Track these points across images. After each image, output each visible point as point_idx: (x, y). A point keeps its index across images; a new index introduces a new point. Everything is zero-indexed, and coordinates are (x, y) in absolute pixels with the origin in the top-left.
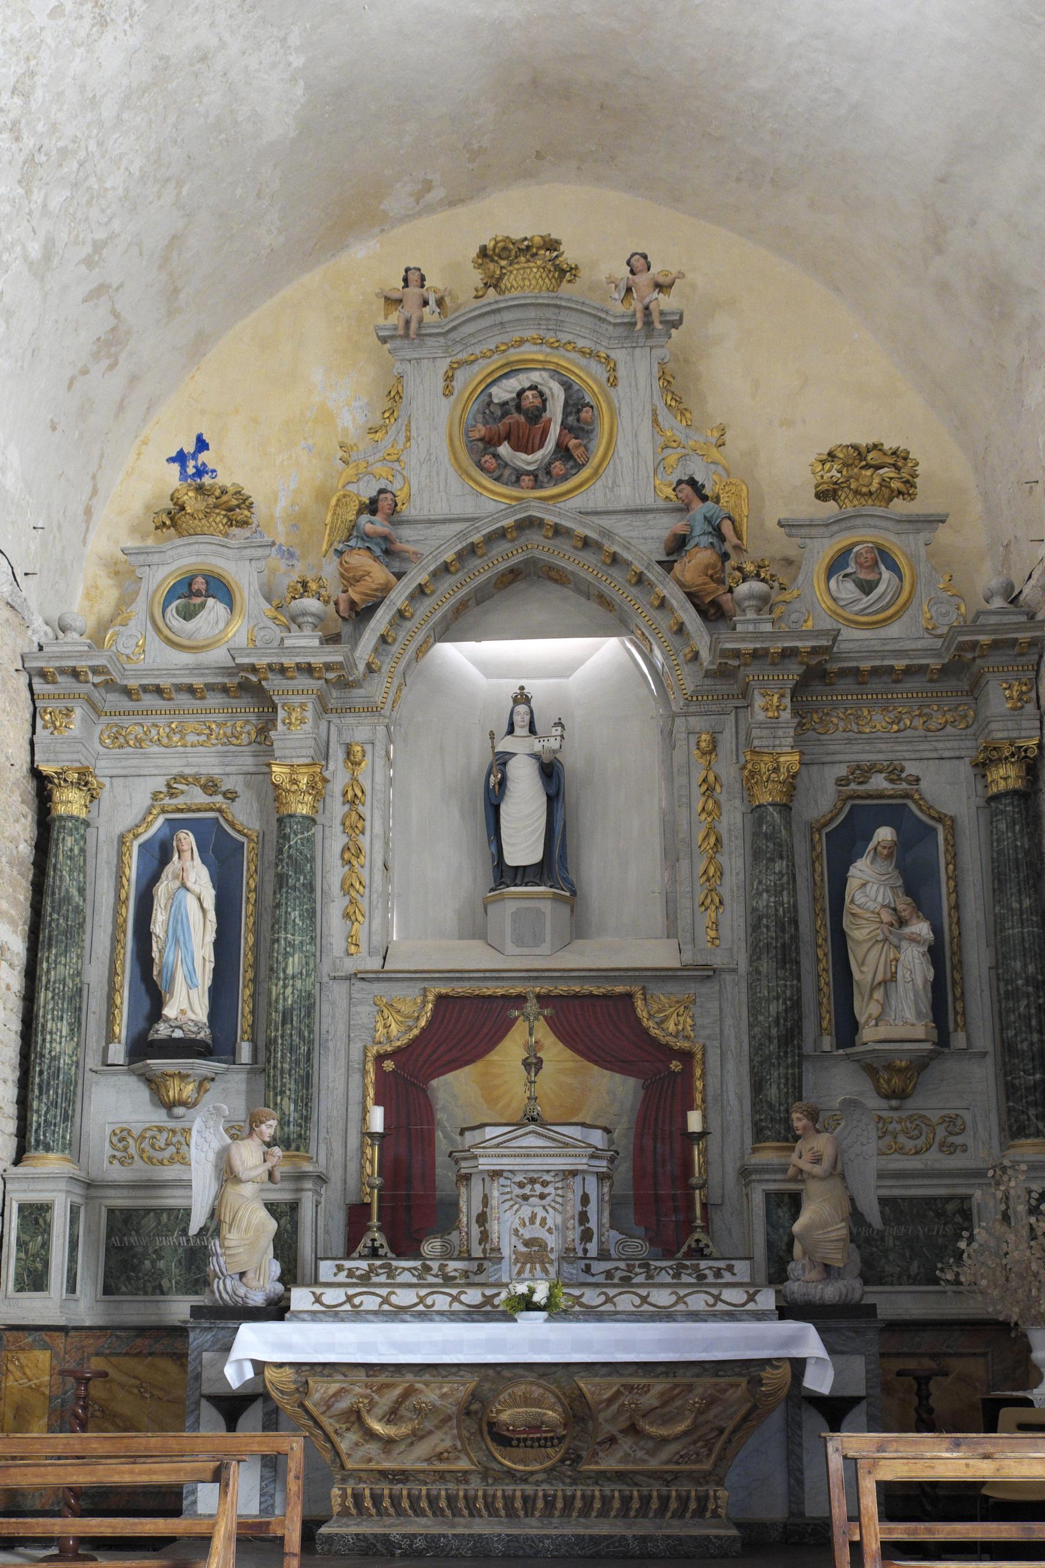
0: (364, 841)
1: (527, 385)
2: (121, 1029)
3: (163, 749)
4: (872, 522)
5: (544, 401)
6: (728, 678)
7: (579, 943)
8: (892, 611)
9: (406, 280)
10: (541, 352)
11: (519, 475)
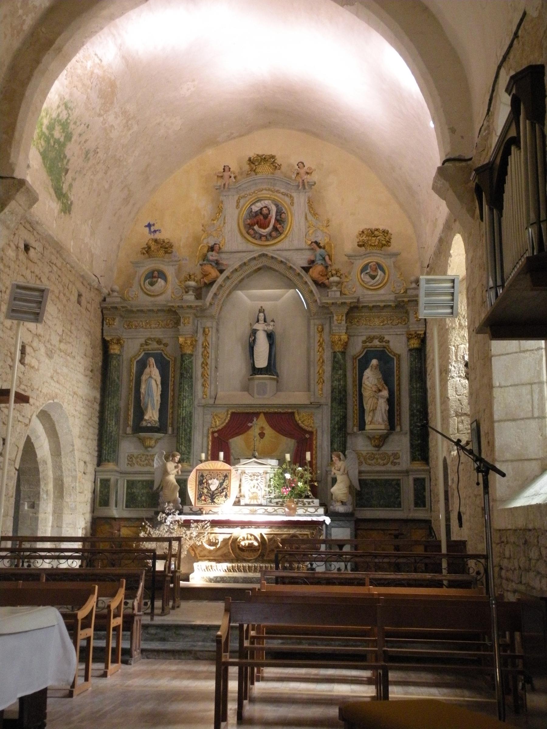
0: (209, 361)
1: (264, 205)
2: (131, 423)
3: (144, 330)
4: (375, 254)
5: (269, 211)
6: (325, 311)
7: (279, 393)
8: (381, 285)
9: (224, 169)
10: (268, 194)
11: (261, 236)
